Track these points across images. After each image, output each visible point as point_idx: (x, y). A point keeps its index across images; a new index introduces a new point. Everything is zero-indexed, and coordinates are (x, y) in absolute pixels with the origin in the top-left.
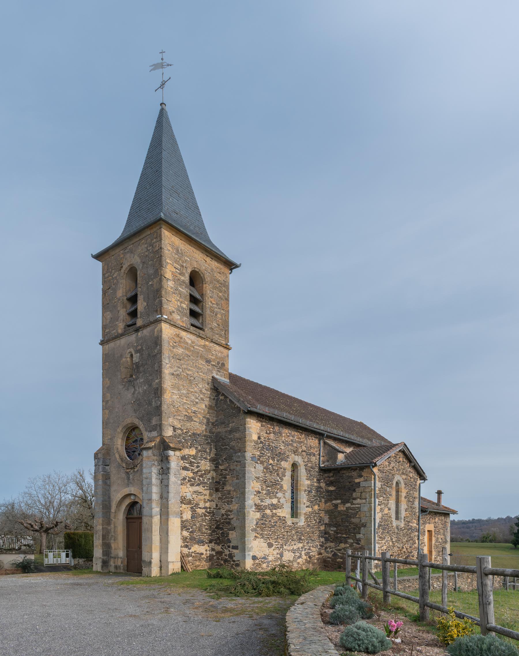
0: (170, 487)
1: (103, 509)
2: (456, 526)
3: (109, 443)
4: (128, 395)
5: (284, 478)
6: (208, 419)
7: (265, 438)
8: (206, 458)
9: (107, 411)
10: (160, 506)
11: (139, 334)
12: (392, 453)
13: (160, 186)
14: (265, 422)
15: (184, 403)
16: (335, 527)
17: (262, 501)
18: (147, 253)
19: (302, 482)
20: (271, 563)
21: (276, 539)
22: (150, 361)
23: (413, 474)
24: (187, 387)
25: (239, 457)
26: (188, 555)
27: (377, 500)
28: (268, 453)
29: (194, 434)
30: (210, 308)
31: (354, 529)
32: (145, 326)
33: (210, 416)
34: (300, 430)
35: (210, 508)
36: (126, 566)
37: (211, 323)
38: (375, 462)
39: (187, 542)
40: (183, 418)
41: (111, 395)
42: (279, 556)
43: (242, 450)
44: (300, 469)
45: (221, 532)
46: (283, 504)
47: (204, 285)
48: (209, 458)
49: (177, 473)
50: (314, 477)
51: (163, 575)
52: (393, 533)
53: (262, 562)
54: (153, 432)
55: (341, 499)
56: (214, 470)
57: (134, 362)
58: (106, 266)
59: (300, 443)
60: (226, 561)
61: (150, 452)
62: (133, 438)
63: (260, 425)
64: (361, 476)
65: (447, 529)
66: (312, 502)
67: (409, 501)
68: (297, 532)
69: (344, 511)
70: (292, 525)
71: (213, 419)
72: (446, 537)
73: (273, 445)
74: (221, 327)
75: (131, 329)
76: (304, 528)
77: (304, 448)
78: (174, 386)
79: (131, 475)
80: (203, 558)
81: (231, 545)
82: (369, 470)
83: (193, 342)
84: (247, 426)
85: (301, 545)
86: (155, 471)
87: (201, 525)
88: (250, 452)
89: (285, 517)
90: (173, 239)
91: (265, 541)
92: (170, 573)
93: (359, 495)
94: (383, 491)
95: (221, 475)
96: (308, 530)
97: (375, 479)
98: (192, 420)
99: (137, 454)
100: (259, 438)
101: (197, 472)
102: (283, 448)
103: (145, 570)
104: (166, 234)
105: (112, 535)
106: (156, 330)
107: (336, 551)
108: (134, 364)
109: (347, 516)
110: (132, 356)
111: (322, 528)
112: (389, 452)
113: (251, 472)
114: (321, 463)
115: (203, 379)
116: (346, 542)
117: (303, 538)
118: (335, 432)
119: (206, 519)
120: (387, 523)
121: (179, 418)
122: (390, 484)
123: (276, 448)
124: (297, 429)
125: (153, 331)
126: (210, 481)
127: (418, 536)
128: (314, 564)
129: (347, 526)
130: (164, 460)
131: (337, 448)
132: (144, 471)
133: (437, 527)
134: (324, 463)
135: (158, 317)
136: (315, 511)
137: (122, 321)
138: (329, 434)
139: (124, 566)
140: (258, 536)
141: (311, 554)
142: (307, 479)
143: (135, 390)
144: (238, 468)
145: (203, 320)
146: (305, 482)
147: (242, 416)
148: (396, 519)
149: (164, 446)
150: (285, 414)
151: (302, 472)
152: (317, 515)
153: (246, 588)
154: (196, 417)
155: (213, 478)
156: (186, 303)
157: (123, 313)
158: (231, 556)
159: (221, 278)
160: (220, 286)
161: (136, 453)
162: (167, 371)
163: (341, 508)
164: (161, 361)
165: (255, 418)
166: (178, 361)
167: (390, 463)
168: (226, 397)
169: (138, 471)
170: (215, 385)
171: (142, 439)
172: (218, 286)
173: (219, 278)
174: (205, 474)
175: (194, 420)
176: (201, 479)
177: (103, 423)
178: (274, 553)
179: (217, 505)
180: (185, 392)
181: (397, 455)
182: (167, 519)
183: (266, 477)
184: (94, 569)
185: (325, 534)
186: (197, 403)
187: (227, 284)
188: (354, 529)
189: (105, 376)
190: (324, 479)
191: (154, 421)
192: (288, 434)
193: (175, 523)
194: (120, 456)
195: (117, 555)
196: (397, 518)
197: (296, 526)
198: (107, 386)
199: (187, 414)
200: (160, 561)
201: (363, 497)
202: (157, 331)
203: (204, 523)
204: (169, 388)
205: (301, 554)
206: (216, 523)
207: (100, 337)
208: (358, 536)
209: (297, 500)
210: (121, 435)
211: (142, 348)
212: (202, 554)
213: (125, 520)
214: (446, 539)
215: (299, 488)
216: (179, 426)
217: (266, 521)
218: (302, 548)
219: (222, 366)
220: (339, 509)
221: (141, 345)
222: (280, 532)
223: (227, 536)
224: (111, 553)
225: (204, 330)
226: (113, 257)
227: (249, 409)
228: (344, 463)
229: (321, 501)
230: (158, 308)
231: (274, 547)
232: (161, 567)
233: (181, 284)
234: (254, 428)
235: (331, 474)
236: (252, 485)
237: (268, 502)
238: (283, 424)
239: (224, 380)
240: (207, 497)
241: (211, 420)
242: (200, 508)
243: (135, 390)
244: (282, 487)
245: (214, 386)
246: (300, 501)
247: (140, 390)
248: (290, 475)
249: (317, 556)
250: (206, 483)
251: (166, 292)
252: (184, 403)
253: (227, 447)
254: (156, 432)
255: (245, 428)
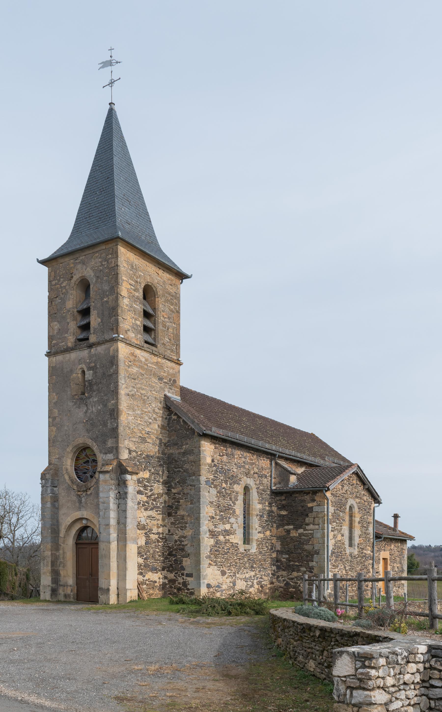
0: (127, 512)
1: (52, 534)
2: (433, 554)
3: (56, 463)
4: (80, 413)
5: (237, 502)
6: (161, 440)
7: (218, 461)
8: (158, 481)
9: (54, 429)
10: (117, 531)
11: (92, 350)
12: (345, 475)
13: (113, 196)
14: (219, 444)
15: (139, 425)
16: (287, 554)
17: (216, 527)
18: (101, 268)
19: (254, 507)
20: (224, 592)
21: (228, 567)
22: (105, 380)
23: (367, 497)
24: (141, 407)
25: (193, 480)
26: (143, 583)
27: (330, 526)
28: (222, 476)
29: (147, 456)
30: (162, 323)
31: (307, 556)
32: (98, 344)
33: (162, 436)
34: (252, 450)
35: (163, 534)
36: (76, 595)
37: (164, 338)
38: (328, 486)
39: (143, 569)
40: (137, 440)
41: (59, 411)
42: (232, 585)
43: (197, 473)
44: (252, 493)
45: (174, 559)
46: (235, 530)
47: (157, 299)
48: (161, 480)
49: (134, 498)
50: (265, 501)
51: (120, 603)
52: (346, 561)
53: (216, 590)
54: (108, 455)
55: (293, 524)
56: (166, 494)
57: (86, 379)
58: (53, 273)
59: (252, 464)
60: (179, 589)
61: (107, 476)
62: (84, 458)
63: (214, 447)
64: (314, 500)
65: (403, 557)
66: (263, 528)
67: (363, 527)
68: (249, 560)
69: (297, 537)
70: (244, 552)
71: (165, 440)
72: (402, 565)
73: (226, 468)
74: (173, 341)
75: (85, 343)
76: (256, 555)
77: (256, 470)
78: (130, 407)
79: (83, 499)
80: (156, 587)
81: (185, 572)
82: (322, 494)
83: (146, 360)
84: (202, 448)
85: (253, 574)
86: (112, 495)
87: (154, 551)
88: (205, 475)
89: (238, 544)
90: (128, 255)
91: (219, 569)
92: (128, 601)
93: (311, 520)
94: (336, 516)
95: (174, 498)
96: (260, 557)
97: (328, 503)
98: (146, 442)
99: (89, 476)
100: (213, 461)
101: (151, 495)
102: (235, 470)
103: (102, 597)
104: (122, 250)
105: (61, 562)
106: (112, 349)
107: (288, 580)
108: (87, 381)
109: (300, 542)
110: (83, 372)
111: (274, 555)
112: (342, 475)
113: (205, 497)
114: (273, 485)
115: (155, 398)
116: (299, 571)
117: (255, 566)
118: (287, 452)
119: (159, 545)
120: (340, 550)
121: (134, 440)
122: (343, 509)
123: (229, 470)
124: (249, 450)
125: (109, 349)
126: (163, 505)
127: (373, 564)
128: (265, 594)
129: (300, 553)
130: (122, 484)
131: (289, 469)
132: (101, 495)
133: (393, 555)
134: (275, 485)
135: (114, 336)
136: (266, 537)
137: (72, 334)
138: (281, 454)
139: (73, 594)
140: (212, 563)
141: (263, 583)
142: (259, 503)
143: (88, 409)
144: (192, 492)
145: (155, 335)
146: (257, 506)
147: (196, 439)
148: (349, 546)
149: (122, 470)
150: (238, 436)
151: (254, 495)
152: (269, 541)
153: (216, 609)
154: (149, 438)
155: (165, 502)
156: (140, 319)
157: (73, 326)
158: (185, 584)
159: (172, 290)
160: (171, 299)
161: (88, 475)
162: (123, 391)
163: (294, 534)
164: (117, 382)
165: (209, 440)
166: (133, 380)
167: (343, 486)
168: (179, 417)
169: (91, 494)
170: (167, 403)
171: (95, 461)
172: (169, 298)
173: (171, 290)
174: (158, 498)
175: (148, 441)
176: (154, 503)
177: (49, 440)
178: (227, 581)
179: (169, 531)
180: (139, 412)
181: (350, 477)
182: (125, 546)
183: (219, 501)
184: (42, 597)
185: (277, 562)
186: (150, 423)
187: (178, 295)
188: (307, 556)
189: (51, 390)
190: (276, 502)
191: (110, 443)
192: (240, 456)
193: (132, 550)
194: (70, 477)
195: (66, 583)
196: (351, 545)
197: (248, 553)
198: (54, 401)
199: (141, 435)
200: (118, 589)
201: (316, 523)
202: (114, 350)
203: (157, 550)
204: (125, 410)
205: (253, 583)
206: (168, 550)
207: (45, 348)
208: (311, 564)
209: (249, 525)
210: (70, 455)
211: (96, 366)
212: (156, 582)
213: (75, 545)
214: (402, 568)
215: (251, 512)
216: (134, 448)
217: (219, 547)
218: (254, 576)
219: (173, 382)
220: (291, 535)
221: (94, 363)
222: (232, 559)
223: (180, 564)
224: (60, 581)
225: (156, 347)
226: (61, 265)
227: (204, 432)
228: (296, 486)
229: (272, 527)
230: (115, 327)
231: (227, 575)
232: (118, 595)
233: (135, 301)
234: (208, 449)
235: (283, 498)
236: (206, 510)
237: (221, 527)
238: (236, 445)
239: (176, 397)
240: (160, 522)
241: (163, 441)
242: (153, 534)
243: (88, 409)
244: (234, 512)
245: (167, 405)
246: (252, 526)
247: (94, 409)
248: (242, 499)
249: (269, 586)
250: (159, 507)
251: (122, 311)
252: (139, 425)
253: (181, 469)
254: (112, 455)
255: (200, 450)
